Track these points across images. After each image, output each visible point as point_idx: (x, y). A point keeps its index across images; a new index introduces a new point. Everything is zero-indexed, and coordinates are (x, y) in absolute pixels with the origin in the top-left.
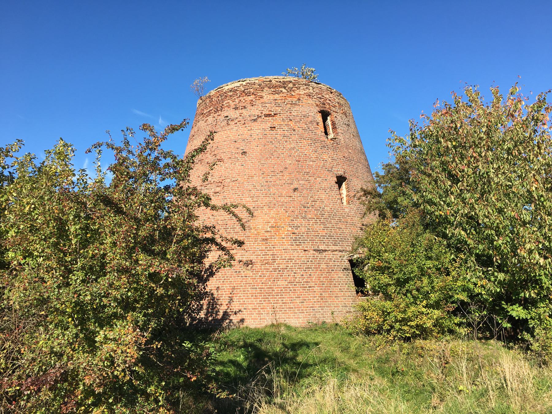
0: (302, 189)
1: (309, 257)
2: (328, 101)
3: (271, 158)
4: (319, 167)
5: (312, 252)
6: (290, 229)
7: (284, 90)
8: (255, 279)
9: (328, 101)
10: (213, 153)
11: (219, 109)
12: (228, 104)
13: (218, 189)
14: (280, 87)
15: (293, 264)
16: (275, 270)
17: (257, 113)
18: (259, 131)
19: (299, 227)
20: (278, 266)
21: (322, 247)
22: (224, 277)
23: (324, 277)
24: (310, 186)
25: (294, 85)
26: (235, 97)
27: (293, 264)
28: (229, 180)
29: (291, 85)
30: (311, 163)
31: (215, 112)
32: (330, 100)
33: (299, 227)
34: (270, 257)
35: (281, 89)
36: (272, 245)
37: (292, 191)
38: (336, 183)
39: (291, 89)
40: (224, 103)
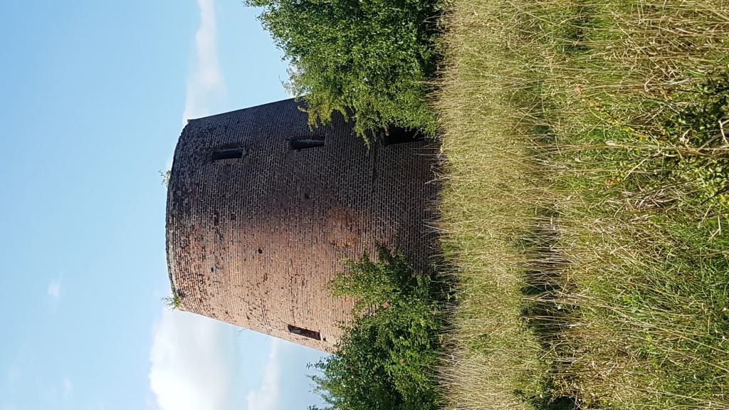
0: (306, 189)
2: (198, 150)
6: (349, 205)
7: (186, 201)
9: (198, 150)
12: (197, 267)
13: (299, 281)
14: (181, 205)
18: (235, 233)
25: (178, 189)
26: (189, 258)
28: (290, 269)
29: (179, 193)
30: (276, 177)
31: (203, 282)
32: (197, 148)
35: (184, 205)
37: (308, 200)
38: (299, 150)
39: (185, 193)
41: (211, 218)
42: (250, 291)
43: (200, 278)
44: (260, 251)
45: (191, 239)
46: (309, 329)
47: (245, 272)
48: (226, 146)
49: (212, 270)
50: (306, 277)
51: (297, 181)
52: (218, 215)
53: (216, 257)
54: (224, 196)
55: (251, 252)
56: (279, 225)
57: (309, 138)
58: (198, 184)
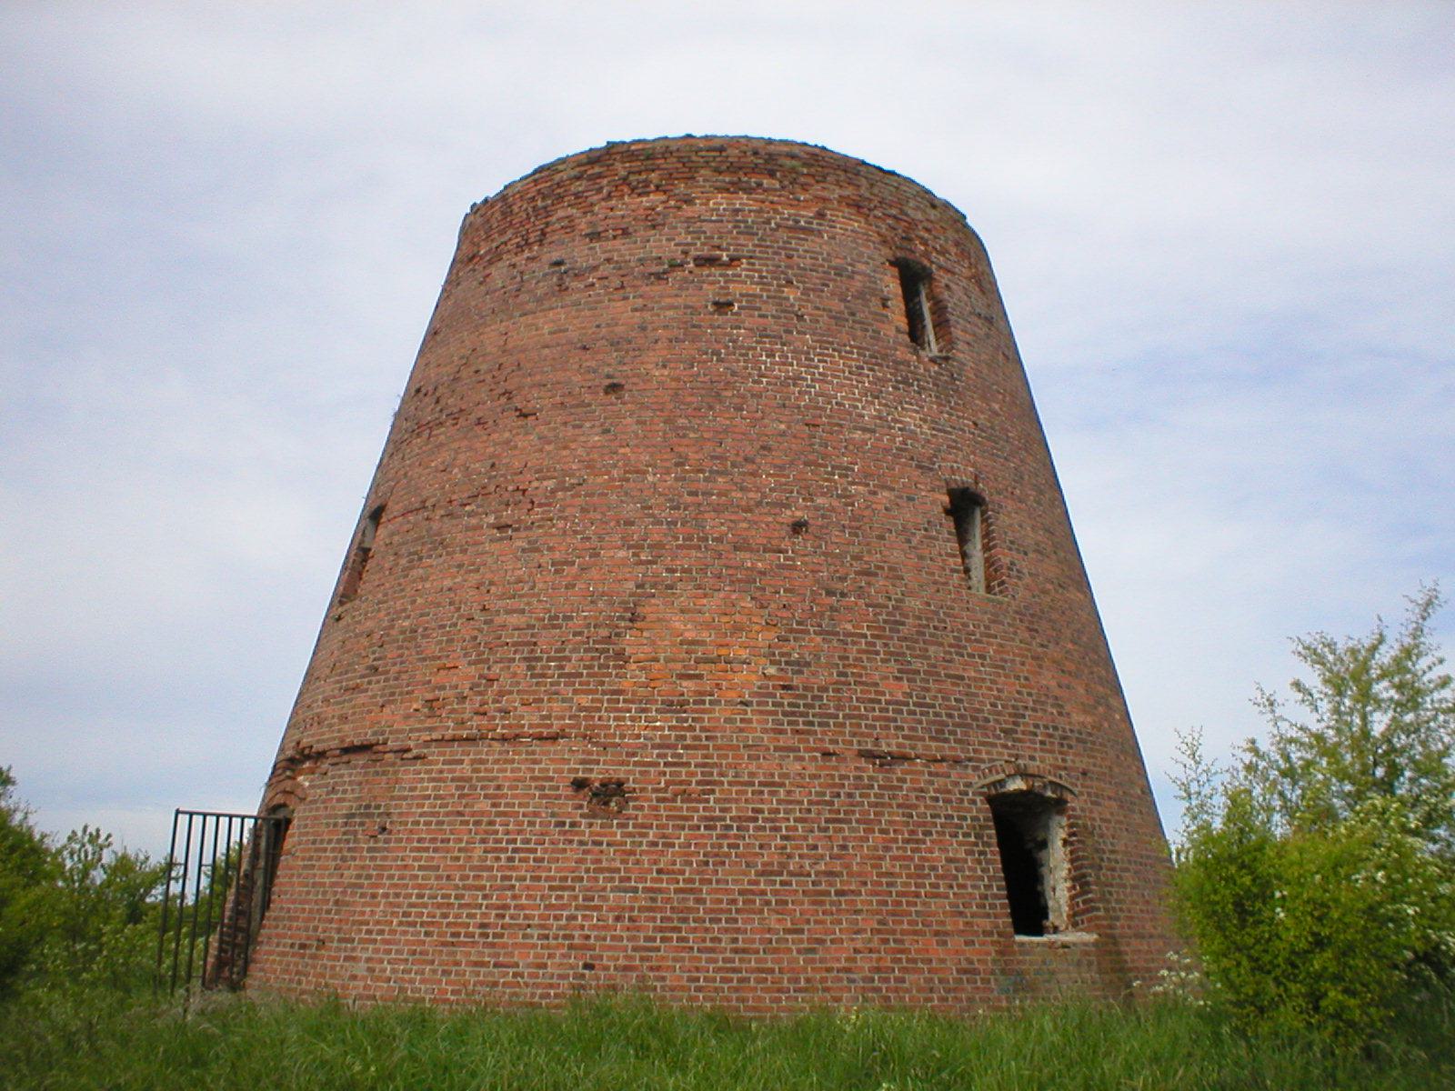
1: (842, 777)
4: (887, 450)
6: (772, 670)
8: (632, 853)
17: (671, 250)
18: (670, 313)
19: (808, 664)
20: (722, 810)
23: (894, 858)
24: (853, 518)
28: (550, 484)
30: (858, 435)
33: (808, 664)
36: (703, 729)
38: (948, 512)
41: (719, 248)
42: (489, 377)
48: (939, 309)
49: (559, 263)
50: (523, 534)
51: (846, 495)
52: (728, 265)
54: (789, 282)
57: (986, 548)
58: (821, 215)
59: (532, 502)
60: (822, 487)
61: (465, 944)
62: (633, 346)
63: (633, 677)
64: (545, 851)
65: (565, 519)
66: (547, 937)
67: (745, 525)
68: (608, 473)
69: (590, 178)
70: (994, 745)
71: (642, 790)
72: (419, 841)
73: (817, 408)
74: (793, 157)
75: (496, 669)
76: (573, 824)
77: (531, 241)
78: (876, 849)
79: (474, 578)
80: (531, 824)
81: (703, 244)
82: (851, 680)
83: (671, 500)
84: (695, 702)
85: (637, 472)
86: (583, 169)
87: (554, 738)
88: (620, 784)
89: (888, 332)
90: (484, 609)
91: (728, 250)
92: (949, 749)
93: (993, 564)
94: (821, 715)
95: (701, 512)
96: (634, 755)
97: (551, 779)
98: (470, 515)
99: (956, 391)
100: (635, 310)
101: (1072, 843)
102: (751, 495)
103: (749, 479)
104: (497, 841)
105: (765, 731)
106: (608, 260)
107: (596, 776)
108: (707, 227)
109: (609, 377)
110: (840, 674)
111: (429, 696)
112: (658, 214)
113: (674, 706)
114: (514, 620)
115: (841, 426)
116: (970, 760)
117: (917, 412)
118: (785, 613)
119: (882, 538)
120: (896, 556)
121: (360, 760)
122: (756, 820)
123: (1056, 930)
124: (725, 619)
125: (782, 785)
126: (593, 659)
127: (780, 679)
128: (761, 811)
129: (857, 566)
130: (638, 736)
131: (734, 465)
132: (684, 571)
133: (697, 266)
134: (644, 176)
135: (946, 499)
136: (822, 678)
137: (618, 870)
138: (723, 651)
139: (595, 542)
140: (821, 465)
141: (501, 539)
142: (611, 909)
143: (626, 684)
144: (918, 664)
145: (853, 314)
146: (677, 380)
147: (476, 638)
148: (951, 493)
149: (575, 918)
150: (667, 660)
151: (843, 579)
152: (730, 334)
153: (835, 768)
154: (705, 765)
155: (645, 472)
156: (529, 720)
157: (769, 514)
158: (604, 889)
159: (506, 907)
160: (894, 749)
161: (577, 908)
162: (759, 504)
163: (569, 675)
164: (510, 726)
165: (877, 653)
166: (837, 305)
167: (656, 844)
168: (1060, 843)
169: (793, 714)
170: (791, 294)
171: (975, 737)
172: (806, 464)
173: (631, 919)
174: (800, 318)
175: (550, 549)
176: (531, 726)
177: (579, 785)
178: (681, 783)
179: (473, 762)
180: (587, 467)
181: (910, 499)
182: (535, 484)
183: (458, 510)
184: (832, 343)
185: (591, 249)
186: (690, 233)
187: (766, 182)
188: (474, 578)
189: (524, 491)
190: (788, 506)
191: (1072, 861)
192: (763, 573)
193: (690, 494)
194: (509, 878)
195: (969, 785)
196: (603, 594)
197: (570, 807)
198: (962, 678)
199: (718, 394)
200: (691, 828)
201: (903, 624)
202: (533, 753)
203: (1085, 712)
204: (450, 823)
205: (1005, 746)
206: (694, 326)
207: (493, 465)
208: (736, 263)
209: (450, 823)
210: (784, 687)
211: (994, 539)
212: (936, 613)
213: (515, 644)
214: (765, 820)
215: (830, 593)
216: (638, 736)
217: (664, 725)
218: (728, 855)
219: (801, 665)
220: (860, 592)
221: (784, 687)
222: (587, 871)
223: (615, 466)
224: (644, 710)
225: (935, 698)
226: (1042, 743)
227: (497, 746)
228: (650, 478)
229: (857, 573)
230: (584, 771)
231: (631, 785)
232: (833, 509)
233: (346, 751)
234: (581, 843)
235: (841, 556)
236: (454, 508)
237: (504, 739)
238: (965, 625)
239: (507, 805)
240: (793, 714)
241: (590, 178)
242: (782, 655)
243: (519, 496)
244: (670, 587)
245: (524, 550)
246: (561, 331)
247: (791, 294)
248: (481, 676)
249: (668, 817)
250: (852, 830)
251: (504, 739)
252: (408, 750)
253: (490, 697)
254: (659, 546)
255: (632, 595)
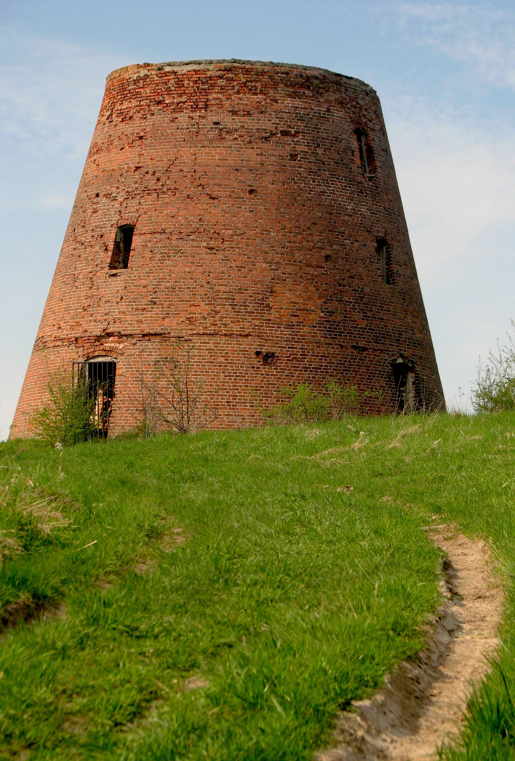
1: (347, 355)
3: (293, 205)
4: (356, 225)
5: (350, 350)
6: (322, 315)
8: (280, 378)
10: (198, 182)
11: (201, 105)
13: (212, 243)
14: (302, 86)
15: (328, 363)
16: (306, 369)
17: (269, 126)
18: (273, 158)
19: (334, 313)
20: (310, 365)
21: (361, 344)
22: (236, 373)
23: (364, 385)
24: (346, 255)
27: (328, 363)
30: (346, 218)
33: (334, 313)
34: (299, 352)
36: (301, 336)
40: (211, 97)
41: (290, 127)
42: (189, 175)
43: (201, 105)
44: (251, 192)
45: (259, 96)
46: (132, 253)
47: (218, 169)
49: (216, 123)
50: (221, 252)
53: (236, 130)
55: (250, 180)
56: (290, 220)
59: (223, 239)
60: (335, 241)
61: (222, 408)
62: (259, 172)
63: (274, 315)
64: (249, 377)
65: (239, 248)
66: (253, 406)
67: (309, 256)
68: (255, 230)
69: (228, 79)
70: (393, 345)
71: (281, 356)
72: (195, 372)
73: (331, 206)
74: (316, 78)
75: (218, 308)
76: (258, 368)
77: (200, 106)
78: (358, 381)
79: (201, 269)
80: (242, 367)
81: (284, 124)
82: (348, 319)
83: (281, 244)
84: (297, 325)
85: (267, 231)
86: (223, 73)
87: (247, 336)
88: (273, 354)
89: (354, 168)
90: (208, 283)
91: (294, 128)
92: (379, 346)
93: (390, 271)
94: (339, 332)
95: (293, 250)
96: (277, 344)
97: (247, 351)
98: (193, 240)
99: (378, 193)
100: (257, 155)
101: (416, 384)
102: (311, 244)
103: (309, 237)
104: (229, 373)
105: (321, 337)
106: (243, 127)
107: (264, 350)
108: (285, 115)
109: (250, 186)
110: (345, 317)
111: (189, 316)
112: (263, 106)
113: (290, 326)
114: (223, 289)
115: (340, 214)
116: (386, 350)
117: (366, 206)
118: (326, 293)
119: (356, 262)
120: (361, 270)
121: (157, 339)
122: (320, 369)
123: (41, 737)
124: (305, 294)
125: (328, 357)
126: (258, 306)
127: (326, 318)
128: (322, 366)
129: (349, 274)
130: (278, 337)
131: (303, 231)
132: (289, 274)
133: (282, 135)
134: (253, 84)
135: (376, 245)
136: (339, 318)
137: (276, 384)
138: (305, 306)
139: (252, 259)
140: (334, 231)
141: (211, 254)
142: (274, 398)
143: (272, 317)
144: (369, 314)
145: (342, 161)
146: (278, 190)
147: (207, 294)
148: (377, 242)
149: (262, 400)
150: (286, 309)
151: (344, 279)
152: (298, 171)
153: (345, 352)
154: (302, 349)
155: (270, 231)
156: (236, 328)
157: (317, 252)
158: (272, 391)
159: (236, 396)
160: (363, 345)
161: (263, 397)
162: (313, 248)
163: (249, 312)
164: (228, 331)
165: (356, 309)
166: (337, 157)
167: (288, 376)
168: (411, 384)
169: (330, 331)
170: (320, 151)
171: (388, 342)
172: (329, 231)
173: (282, 401)
174: (324, 163)
175: (234, 260)
176: (237, 331)
177: (258, 353)
178: (294, 355)
179: (214, 343)
180: (246, 226)
181: (365, 245)
182: (223, 231)
183: (185, 237)
184: (335, 175)
185: (233, 119)
186: (278, 118)
187: (307, 92)
188: (201, 269)
189: (219, 234)
190: (323, 249)
191: (415, 390)
192: (317, 276)
193: (288, 242)
194: (236, 386)
195: (386, 360)
196: (259, 281)
197: (257, 362)
198: (383, 319)
199: (295, 199)
200: (300, 371)
201: (364, 298)
202: (239, 341)
203: (421, 333)
204: (208, 366)
205: (397, 346)
206: (283, 166)
207: (200, 219)
208: (297, 135)
209: (208, 366)
210: (327, 321)
211: (391, 261)
212: (374, 293)
213: (225, 298)
214: (324, 369)
215: (340, 285)
216: (278, 337)
217: (287, 332)
218: (312, 381)
219: (331, 313)
220: (350, 285)
221: (327, 321)
222: (265, 384)
223: (257, 227)
224: (279, 327)
225: (375, 327)
226: (408, 345)
227: (224, 338)
228: (272, 234)
229: (348, 277)
230: (260, 349)
231: (277, 355)
232: (339, 251)
233: (144, 336)
234: (262, 374)
235: (343, 270)
236: (183, 235)
237: (226, 335)
238: (383, 298)
239: (231, 360)
240: (330, 331)
241: (228, 79)
242: (325, 309)
243: (216, 236)
244: (284, 280)
245: (222, 260)
246: (224, 160)
247: (320, 151)
248: (212, 310)
249: (292, 367)
250: (351, 374)
251: (226, 335)
252: (183, 337)
253: (217, 318)
254: (278, 263)
255: (270, 282)
